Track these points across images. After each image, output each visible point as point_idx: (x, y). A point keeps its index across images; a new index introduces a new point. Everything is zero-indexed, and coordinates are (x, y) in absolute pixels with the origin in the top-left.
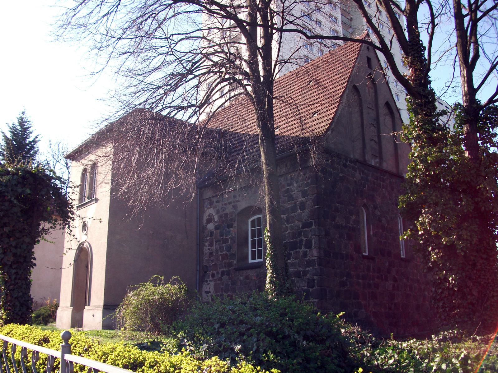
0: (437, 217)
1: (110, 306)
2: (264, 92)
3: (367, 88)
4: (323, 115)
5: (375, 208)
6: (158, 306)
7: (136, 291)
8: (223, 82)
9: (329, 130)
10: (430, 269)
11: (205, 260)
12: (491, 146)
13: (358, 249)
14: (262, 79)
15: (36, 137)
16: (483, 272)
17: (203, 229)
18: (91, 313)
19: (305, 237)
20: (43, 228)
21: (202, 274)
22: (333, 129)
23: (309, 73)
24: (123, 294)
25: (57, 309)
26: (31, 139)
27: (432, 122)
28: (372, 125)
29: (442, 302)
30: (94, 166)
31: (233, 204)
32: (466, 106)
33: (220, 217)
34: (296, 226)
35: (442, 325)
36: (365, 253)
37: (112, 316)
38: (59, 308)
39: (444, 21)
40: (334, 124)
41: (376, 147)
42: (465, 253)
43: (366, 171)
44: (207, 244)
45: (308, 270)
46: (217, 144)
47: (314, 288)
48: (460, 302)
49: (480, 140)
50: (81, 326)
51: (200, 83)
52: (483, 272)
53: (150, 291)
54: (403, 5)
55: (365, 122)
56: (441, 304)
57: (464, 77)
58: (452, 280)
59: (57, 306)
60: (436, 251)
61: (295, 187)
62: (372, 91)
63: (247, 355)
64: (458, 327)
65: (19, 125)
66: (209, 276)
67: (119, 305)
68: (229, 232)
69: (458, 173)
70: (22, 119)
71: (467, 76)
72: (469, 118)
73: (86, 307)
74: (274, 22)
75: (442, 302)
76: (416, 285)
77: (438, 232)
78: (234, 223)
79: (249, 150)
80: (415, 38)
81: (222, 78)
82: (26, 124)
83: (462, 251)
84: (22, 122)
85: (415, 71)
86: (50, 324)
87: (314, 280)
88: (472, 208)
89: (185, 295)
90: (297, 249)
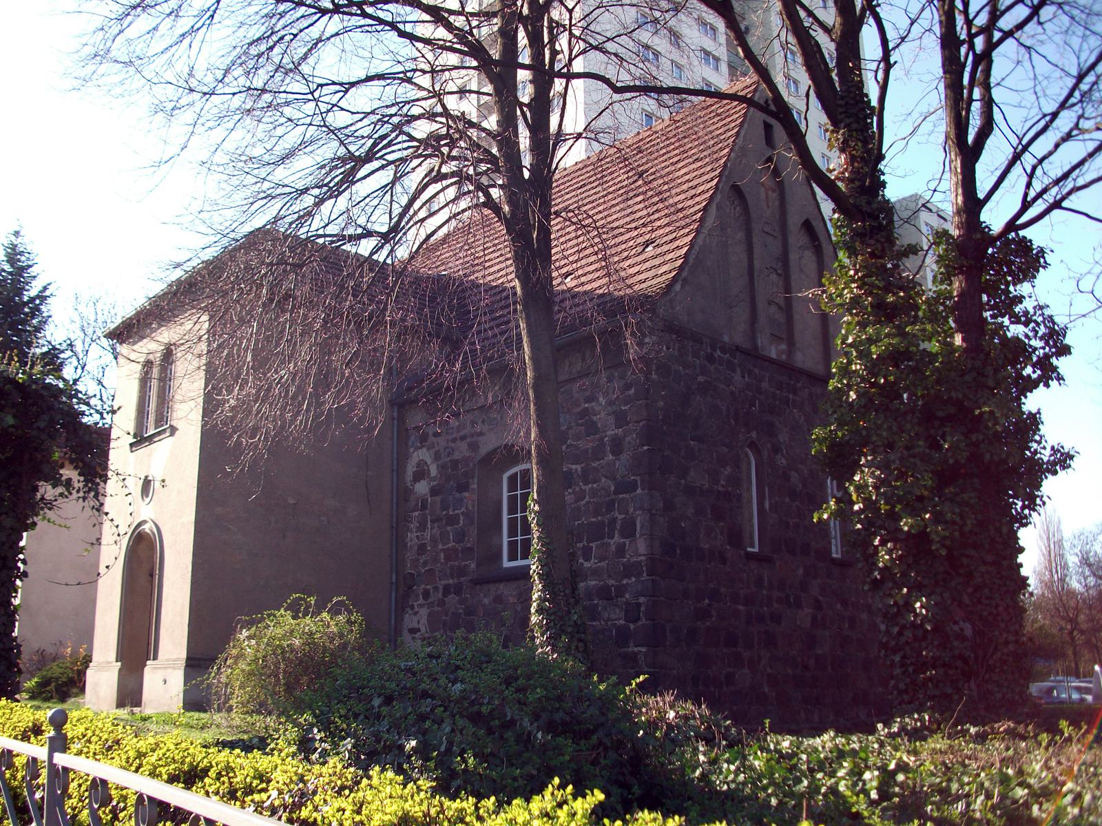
0: (891, 473)
1: (199, 659)
2: (528, 205)
3: (763, 189)
4: (665, 248)
5: (776, 450)
6: (301, 661)
7: (254, 629)
8: (436, 182)
9: (677, 281)
10: (876, 584)
11: (408, 561)
12: (1012, 323)
13: (736, 537)
14: (526, 174)
15: (45, 288)
16: (987, 591)
17: (404, 493)
18: (160, 675)
19: (620, 513)
20: (43, 496)
21: (405, 590)
22: (685, 281)
23: (625, 162)
24: (226, 636)
25: (87, 667)
26: (33, 293)
27: (886, 269)
28: (771, 270)
29: (902, 653)
30: (168, 355)
31: (469, 440)
32: (958, 237)
33: (442, 468)
34: (603, 488)
35: (900, 704)
36: (753, 547)
37: (202, 682)
38: (91, 664)
39: (930, 46)
40: (687, 269)
41: (780, 317)
42: (949, 550)
43: (757, 371)
44: (414, 525)
45: (627, 584)
46: (437, 304)
47: (640, 623)
48: (937, 653)
49: (989, 310)
50: (138, 703)
51: (396, 179)
52: (987, 591)
53: (287, 628)
54: (830, 16)
55: (757, 264)
56: (897, 658)
57: (956, 174)
58: (922, 607)
59: (87, 660)
60: (889, 545)
61: (601, 404)
62: (774, 196)
63: (427, 759)
64: (932, 708)
65: (8, 261)
66: (417, 596)
67: (217, 658)
68: (462, 500)
69: (938, 382)
70: (14, 247)
71: (962, 172)
72: (965, 263)
73: (148, 662)
74: (558, 47)
75: (902, 653)
76: (864, 616)
77: (893, 507)
78: (471, 481)
79: (485, 330)
80: (853, 89)
81: (434, 174)
82: (23, 258)
83: (944, 546)
84: (13, 255)
85: (852, 159)
86: (73, 700)
87: (639, 605)
88: (965, 454)
89: (361, 637)
90: (603, 538)
